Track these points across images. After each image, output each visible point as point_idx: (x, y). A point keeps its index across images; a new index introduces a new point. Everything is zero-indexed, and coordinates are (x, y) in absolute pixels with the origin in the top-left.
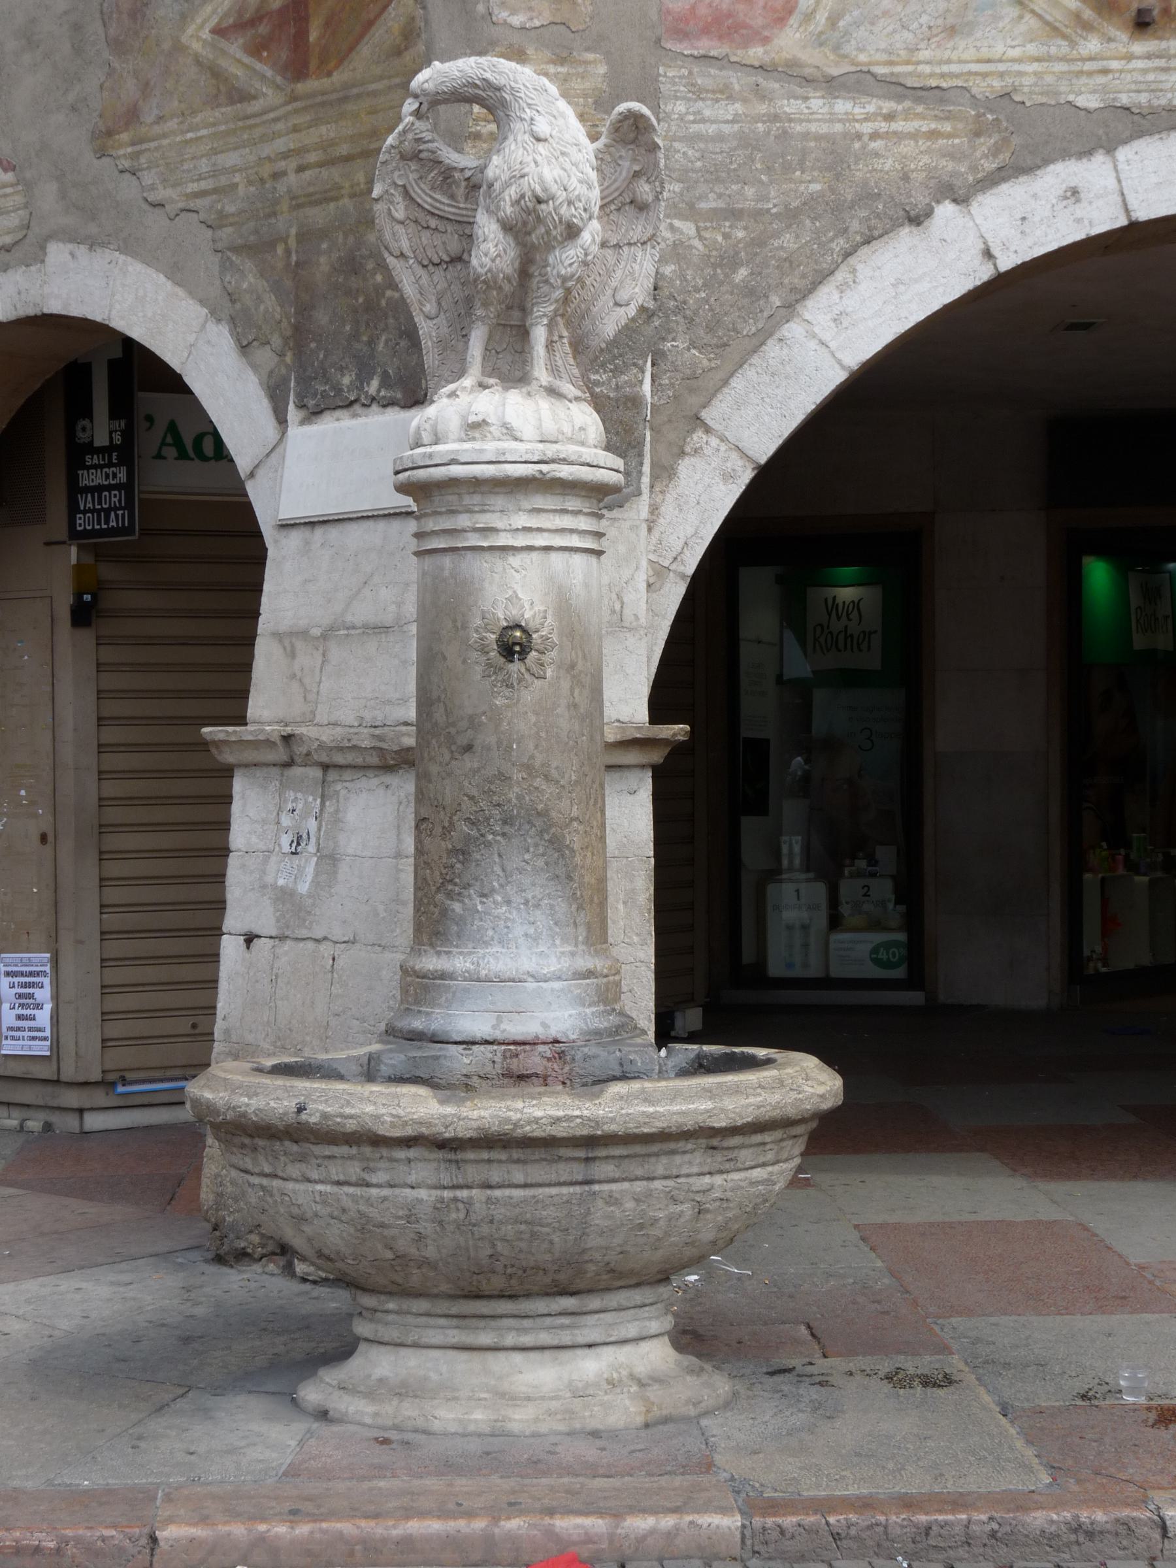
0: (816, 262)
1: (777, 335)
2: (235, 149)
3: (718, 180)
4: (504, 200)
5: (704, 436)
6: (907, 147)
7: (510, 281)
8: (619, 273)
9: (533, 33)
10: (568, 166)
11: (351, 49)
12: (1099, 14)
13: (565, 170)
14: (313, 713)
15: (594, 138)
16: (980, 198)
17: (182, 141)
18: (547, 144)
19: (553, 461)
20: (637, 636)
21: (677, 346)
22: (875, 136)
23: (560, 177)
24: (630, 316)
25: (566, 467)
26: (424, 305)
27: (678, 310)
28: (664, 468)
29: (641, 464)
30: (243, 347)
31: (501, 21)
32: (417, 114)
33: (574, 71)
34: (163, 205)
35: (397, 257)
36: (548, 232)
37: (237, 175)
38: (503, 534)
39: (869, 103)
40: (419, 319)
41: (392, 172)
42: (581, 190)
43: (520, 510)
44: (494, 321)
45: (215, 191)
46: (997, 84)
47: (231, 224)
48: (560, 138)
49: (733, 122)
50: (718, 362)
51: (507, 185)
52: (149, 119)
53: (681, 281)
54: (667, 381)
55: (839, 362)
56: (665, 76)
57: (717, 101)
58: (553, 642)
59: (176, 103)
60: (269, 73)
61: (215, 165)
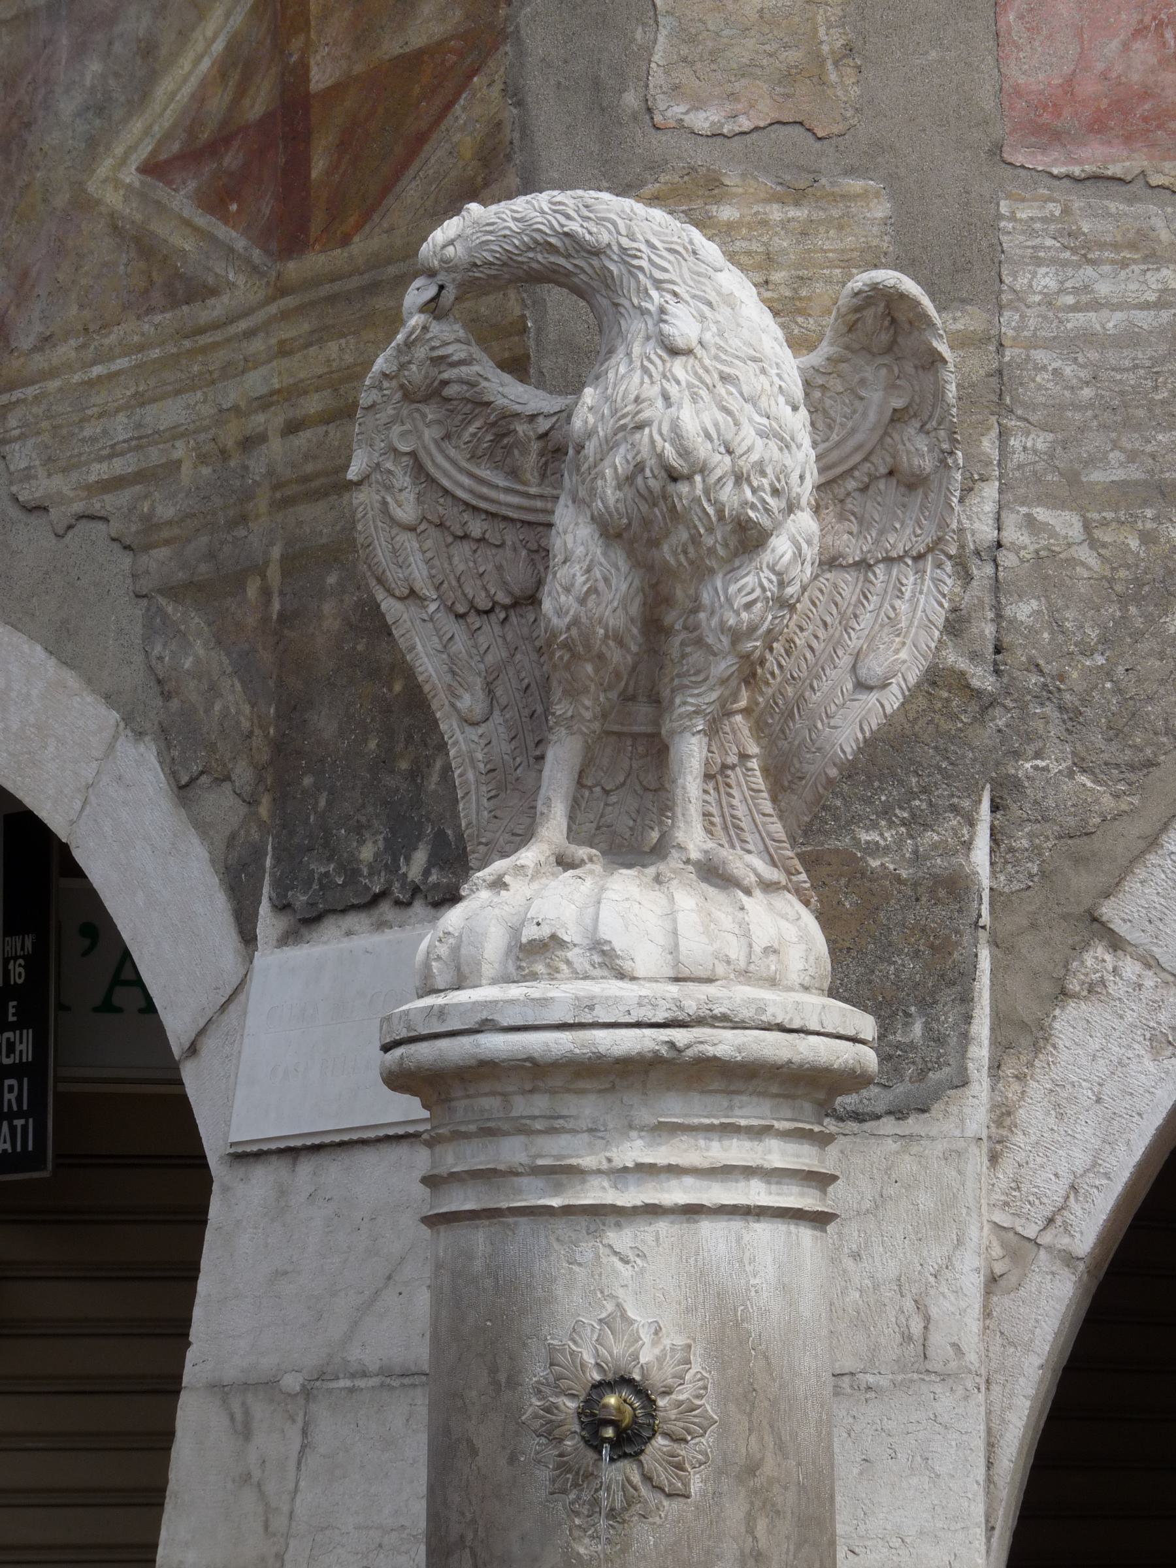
2: (178, 392)
3: (1129, 424)
4: (603, 477)
5: (1108, 957)
7: (621, 643)
8: (866, 619)
9: (736, 143)
10: (734, 404)
11: (386, 190)
13: (728, 411)
15: (798, 343)
17: (83, 383)
18: (691, 360)
19: (700, 1022)
21: (1046, 769)
23: (716, 425)
24: (889, 710)
25: (728, 1034)
26: (459, 697)
27: (1047, 693)
29: (968, 1018)
30: (181, 788)
31: (672, 123)
32: (432, 307)
33: (822, 215)
34: (45, 509)
35: (401, 599)
36: (695, 539)
37: (179, 444)
38: (595, 1181)
40: (448, 726)
41: (388, 426)
42: (770, 451)
43: (631, 1127)
44: (596, 726)
45: (139, 477)
47: (167, 542)
48: (719, 348)
50: (1136, 800)
51: (610, 446)
52: (26, 343)
53: (1052, 633)
54: (1025, 843)
56: (1013, 218)
57: (1124, 264)
58: (703, 1416)
59: (74, 310)
60: (240, 244)
61: (139, 426)
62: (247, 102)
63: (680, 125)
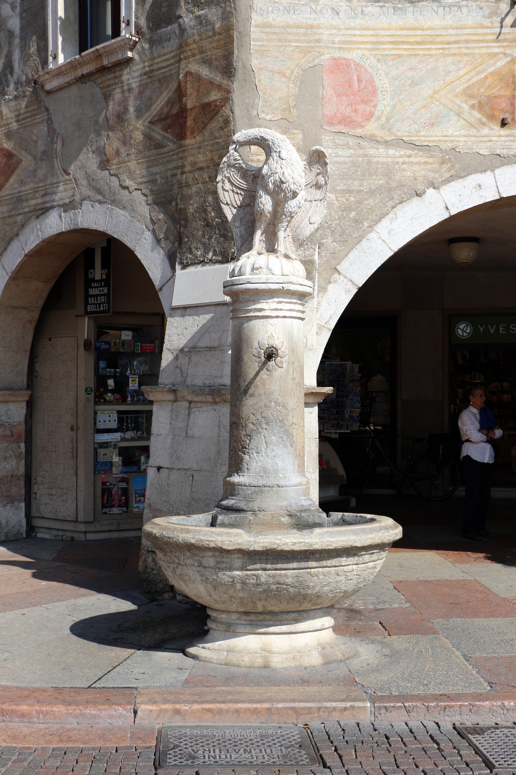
0: (381, 210)
1: (367, 237)
2: (157, 166)
6: (416, 168)
7: (270, 213)
9: (274, 122)
12: (488, 120)
14: (185, 381)
16: (444, 187)
20: (313, 352)
22: (403, 163)
27: (328, 227)
28: (323, 288)
39: (401, 151)
46: (450, 145)
49: (350, 157)
54: (324, 255)
55: (390, 248)
56: (324, 139)
57: (344, 149)
60: (171, 138)
62: (172, 110)
63: (264, 118)
